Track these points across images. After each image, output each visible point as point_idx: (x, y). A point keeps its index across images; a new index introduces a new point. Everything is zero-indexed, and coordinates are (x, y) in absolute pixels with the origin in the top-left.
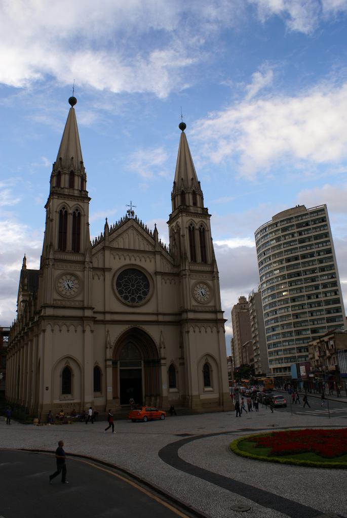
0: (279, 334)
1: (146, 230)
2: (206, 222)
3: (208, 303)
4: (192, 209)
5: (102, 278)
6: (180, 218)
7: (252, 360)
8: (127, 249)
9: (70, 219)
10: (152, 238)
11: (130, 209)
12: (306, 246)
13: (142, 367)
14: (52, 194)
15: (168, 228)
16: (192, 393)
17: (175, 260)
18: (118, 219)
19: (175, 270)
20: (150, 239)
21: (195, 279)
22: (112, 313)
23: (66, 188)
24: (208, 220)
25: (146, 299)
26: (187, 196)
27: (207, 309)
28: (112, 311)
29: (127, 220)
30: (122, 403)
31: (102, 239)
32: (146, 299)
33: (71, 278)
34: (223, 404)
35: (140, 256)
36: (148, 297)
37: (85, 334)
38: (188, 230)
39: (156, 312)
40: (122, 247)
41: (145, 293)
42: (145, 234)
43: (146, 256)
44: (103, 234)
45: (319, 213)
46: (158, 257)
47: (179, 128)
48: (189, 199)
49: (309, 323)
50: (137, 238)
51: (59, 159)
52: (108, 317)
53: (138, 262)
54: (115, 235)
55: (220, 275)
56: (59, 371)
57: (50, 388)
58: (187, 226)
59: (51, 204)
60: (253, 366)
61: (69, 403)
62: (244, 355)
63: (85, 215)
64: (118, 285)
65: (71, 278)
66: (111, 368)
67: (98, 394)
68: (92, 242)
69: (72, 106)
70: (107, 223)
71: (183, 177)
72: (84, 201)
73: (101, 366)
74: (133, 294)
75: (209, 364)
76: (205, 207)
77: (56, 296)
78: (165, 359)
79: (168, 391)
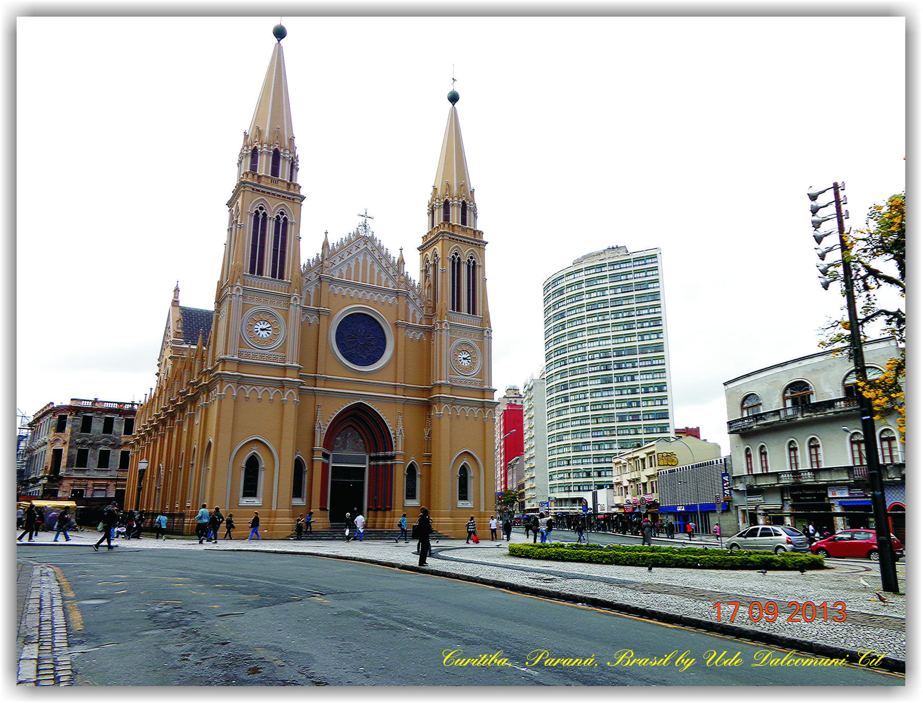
0: (567, 445)
6: (440, 242)
7: (522, 486)
9: (464, 268)
14: (241, 185)
18: (345, 235)
24: (481, 250)
30: (332, 520)
31: (320, 263)
48: (455, 216)
49: (636, 338)
60: (522, 495)
62: (509, 478)
68: (302, 267)
76: (479, 228)
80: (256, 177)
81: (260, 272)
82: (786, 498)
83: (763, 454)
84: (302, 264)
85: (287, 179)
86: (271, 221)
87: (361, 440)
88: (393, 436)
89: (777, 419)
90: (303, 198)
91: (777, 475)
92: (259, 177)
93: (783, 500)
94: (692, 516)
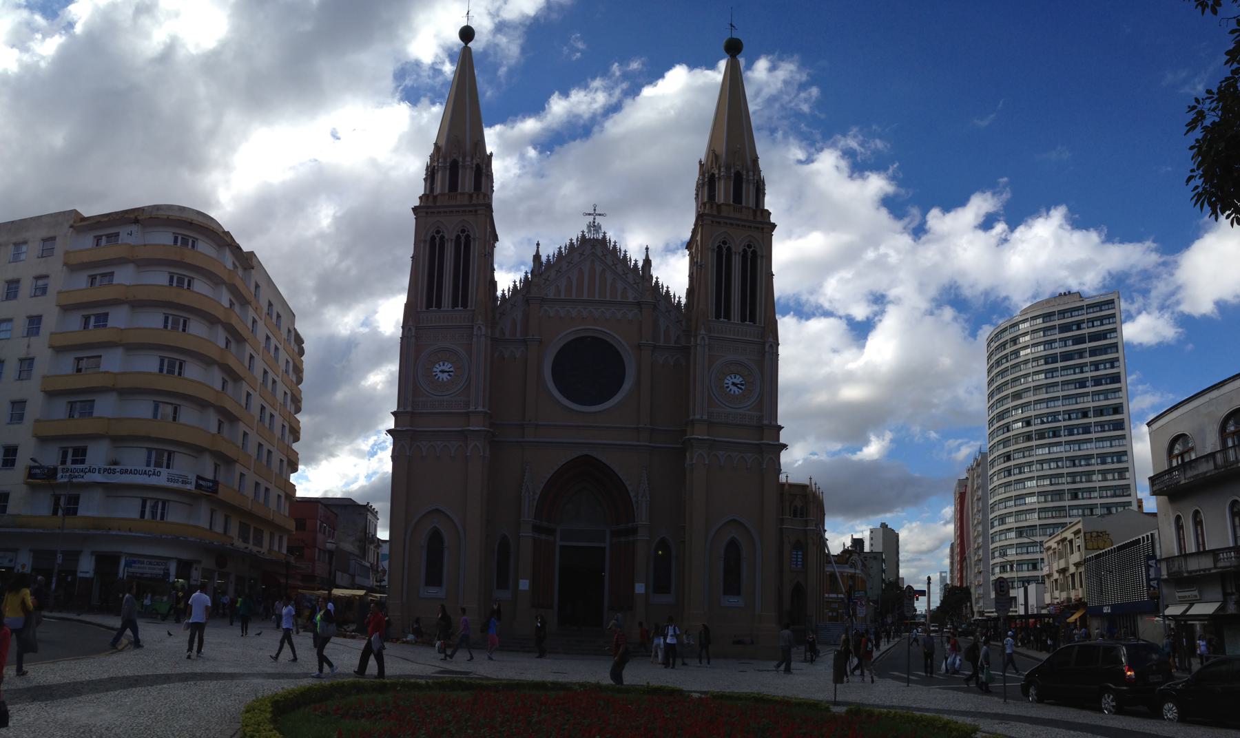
11: (592, 220)
12: (1073, 367)
14: (700, 217)
15: (411, 262)
45: (1103, 308)
47: (742, 40)
70: (538, 251)
80: (715, 206)
81: (728, 316)
82: (1230, 591)
83: (1198, 523)
84: (499, 293)
85: (752, 204)
86: (737, 256)
88: (634, 500)
89: (1211, 466)
91: (1215, 553)
92: (719, 206)
93: (1225, 594)
94: (272, 535)
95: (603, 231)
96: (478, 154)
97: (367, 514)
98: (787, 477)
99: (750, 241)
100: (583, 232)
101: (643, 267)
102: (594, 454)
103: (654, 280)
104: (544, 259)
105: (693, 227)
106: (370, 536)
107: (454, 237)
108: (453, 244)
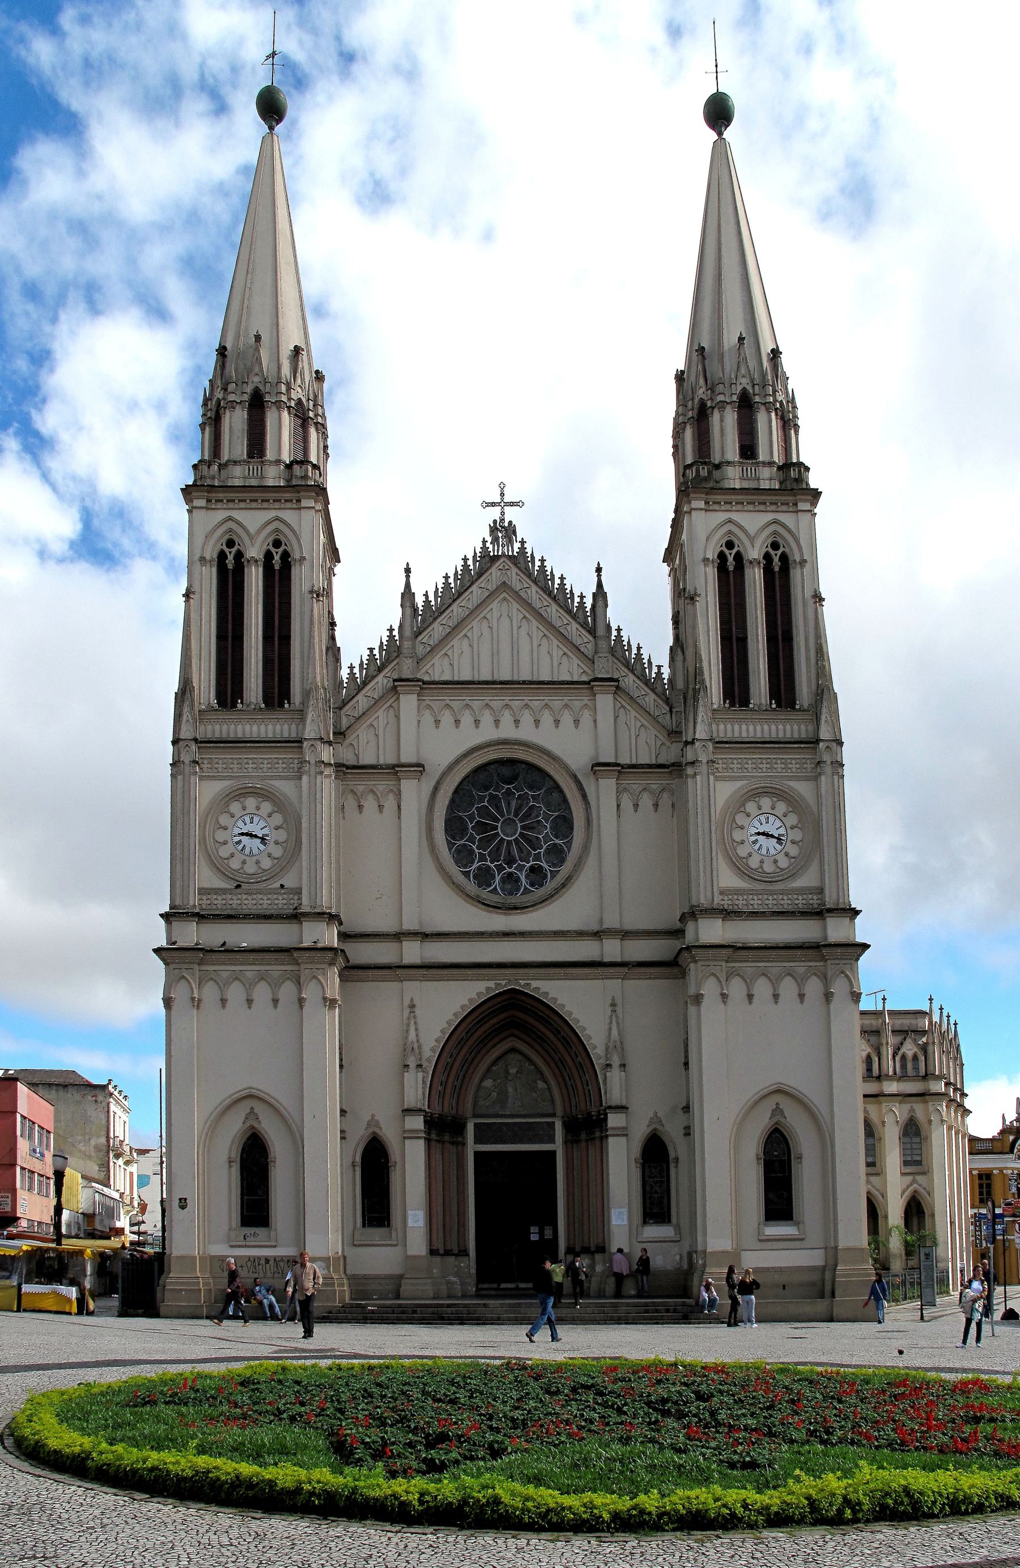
1: (561, 596)
2: (791, 525)
3: (793, 876)
4: (733, 477)
5: (390, 803)
8: (524, 682)
10: (584, 625)
13: (558, 1146)
14: (685, 490)
16: (705, 1243)
17: (674, 710)
18: (452, 565)
19: (670, 754)
20: (573, 629)
21: (741, 778)
22: (425, 936)
23: (235, 462)
24: (804, 518)
25: (559, 878)
26: (715, 418)
27: (786, 903)
28: (428, 930)
29: (486, 560)
32: (559, 878)
33: (258, 808)
34: (833, 1295)
35: (455, 705)
36: (565, 869)
37: (832, 1006)
38: (712, 573)
39: (595, 927)
40: (466, 676)
41: (558, 855)
42: (553, 612)
43: (557, 702)
44: (396, 633)
46: (605, 701)
50: (523, 632)
51: (698, 352)
52: (412, 952)
53: (526, 732)
54: (437, 630)
55: (848, 754)
56: (752, 1147)
57: (193, 1204)
58: (712, 554)
59: (684, 537)
61: (259, 1258)
63: (803, 562)
64: (454, 827)
65: (258, 808)
66: (421, 1144)
67: (377, 1233)
69: (720, 134)
70: (408, 585)
71: (705, 344)
72: (299, 501)
73: (390, 1135)
74: (510, 862)
75: (378, 1134)
77: (728, 879)
78: (622, 1108)
79: (759, 1232)
84: (344, 673)
87: (541, 1085)
90: (816, 494)
95: (519, 539)
96: (299, 381)
97: (108, 1104)
98: (884, 999)
99: (775, 533)
100: (484, 542)
101: (594, 606)
102: (520, 985)
103: (614, 633)
104: (420, 601)
105: (673, 516)
106: (117, 1143)
107: (261, 556)
108: (261, 570)
